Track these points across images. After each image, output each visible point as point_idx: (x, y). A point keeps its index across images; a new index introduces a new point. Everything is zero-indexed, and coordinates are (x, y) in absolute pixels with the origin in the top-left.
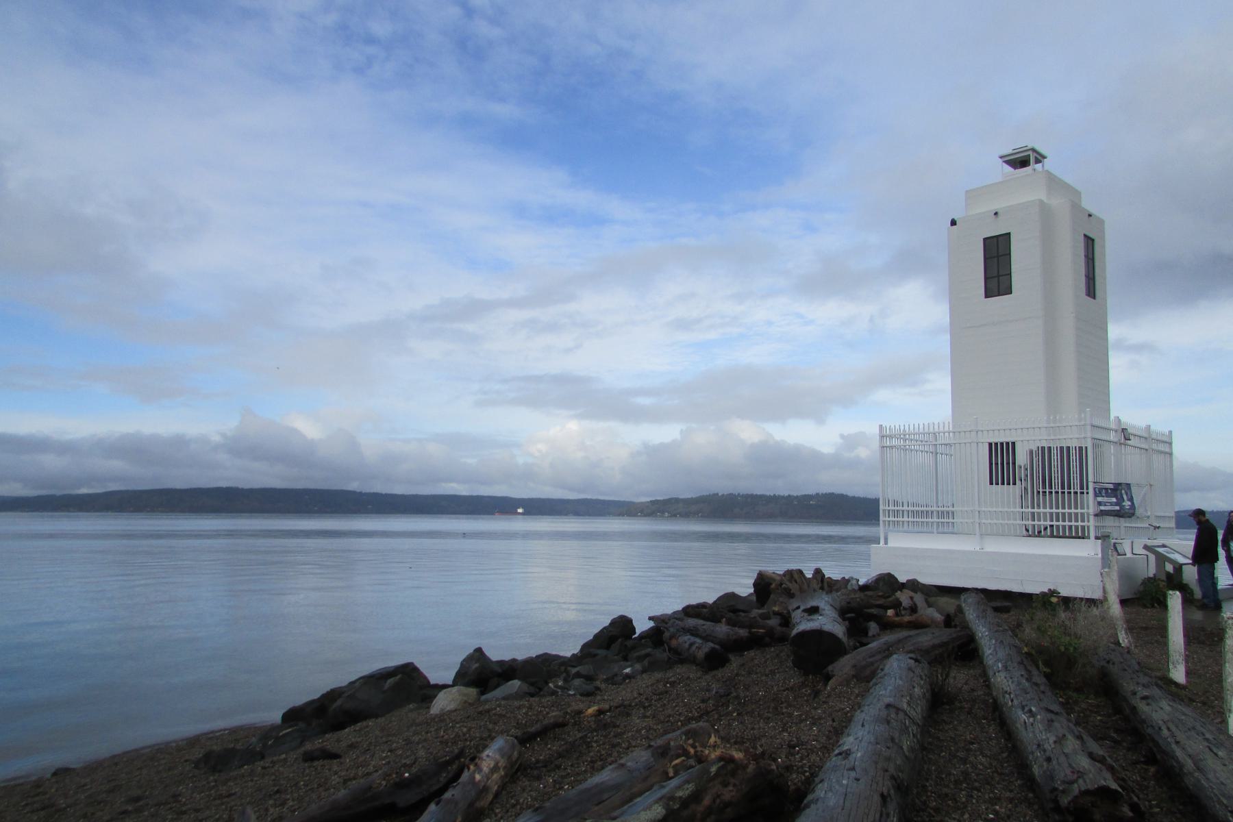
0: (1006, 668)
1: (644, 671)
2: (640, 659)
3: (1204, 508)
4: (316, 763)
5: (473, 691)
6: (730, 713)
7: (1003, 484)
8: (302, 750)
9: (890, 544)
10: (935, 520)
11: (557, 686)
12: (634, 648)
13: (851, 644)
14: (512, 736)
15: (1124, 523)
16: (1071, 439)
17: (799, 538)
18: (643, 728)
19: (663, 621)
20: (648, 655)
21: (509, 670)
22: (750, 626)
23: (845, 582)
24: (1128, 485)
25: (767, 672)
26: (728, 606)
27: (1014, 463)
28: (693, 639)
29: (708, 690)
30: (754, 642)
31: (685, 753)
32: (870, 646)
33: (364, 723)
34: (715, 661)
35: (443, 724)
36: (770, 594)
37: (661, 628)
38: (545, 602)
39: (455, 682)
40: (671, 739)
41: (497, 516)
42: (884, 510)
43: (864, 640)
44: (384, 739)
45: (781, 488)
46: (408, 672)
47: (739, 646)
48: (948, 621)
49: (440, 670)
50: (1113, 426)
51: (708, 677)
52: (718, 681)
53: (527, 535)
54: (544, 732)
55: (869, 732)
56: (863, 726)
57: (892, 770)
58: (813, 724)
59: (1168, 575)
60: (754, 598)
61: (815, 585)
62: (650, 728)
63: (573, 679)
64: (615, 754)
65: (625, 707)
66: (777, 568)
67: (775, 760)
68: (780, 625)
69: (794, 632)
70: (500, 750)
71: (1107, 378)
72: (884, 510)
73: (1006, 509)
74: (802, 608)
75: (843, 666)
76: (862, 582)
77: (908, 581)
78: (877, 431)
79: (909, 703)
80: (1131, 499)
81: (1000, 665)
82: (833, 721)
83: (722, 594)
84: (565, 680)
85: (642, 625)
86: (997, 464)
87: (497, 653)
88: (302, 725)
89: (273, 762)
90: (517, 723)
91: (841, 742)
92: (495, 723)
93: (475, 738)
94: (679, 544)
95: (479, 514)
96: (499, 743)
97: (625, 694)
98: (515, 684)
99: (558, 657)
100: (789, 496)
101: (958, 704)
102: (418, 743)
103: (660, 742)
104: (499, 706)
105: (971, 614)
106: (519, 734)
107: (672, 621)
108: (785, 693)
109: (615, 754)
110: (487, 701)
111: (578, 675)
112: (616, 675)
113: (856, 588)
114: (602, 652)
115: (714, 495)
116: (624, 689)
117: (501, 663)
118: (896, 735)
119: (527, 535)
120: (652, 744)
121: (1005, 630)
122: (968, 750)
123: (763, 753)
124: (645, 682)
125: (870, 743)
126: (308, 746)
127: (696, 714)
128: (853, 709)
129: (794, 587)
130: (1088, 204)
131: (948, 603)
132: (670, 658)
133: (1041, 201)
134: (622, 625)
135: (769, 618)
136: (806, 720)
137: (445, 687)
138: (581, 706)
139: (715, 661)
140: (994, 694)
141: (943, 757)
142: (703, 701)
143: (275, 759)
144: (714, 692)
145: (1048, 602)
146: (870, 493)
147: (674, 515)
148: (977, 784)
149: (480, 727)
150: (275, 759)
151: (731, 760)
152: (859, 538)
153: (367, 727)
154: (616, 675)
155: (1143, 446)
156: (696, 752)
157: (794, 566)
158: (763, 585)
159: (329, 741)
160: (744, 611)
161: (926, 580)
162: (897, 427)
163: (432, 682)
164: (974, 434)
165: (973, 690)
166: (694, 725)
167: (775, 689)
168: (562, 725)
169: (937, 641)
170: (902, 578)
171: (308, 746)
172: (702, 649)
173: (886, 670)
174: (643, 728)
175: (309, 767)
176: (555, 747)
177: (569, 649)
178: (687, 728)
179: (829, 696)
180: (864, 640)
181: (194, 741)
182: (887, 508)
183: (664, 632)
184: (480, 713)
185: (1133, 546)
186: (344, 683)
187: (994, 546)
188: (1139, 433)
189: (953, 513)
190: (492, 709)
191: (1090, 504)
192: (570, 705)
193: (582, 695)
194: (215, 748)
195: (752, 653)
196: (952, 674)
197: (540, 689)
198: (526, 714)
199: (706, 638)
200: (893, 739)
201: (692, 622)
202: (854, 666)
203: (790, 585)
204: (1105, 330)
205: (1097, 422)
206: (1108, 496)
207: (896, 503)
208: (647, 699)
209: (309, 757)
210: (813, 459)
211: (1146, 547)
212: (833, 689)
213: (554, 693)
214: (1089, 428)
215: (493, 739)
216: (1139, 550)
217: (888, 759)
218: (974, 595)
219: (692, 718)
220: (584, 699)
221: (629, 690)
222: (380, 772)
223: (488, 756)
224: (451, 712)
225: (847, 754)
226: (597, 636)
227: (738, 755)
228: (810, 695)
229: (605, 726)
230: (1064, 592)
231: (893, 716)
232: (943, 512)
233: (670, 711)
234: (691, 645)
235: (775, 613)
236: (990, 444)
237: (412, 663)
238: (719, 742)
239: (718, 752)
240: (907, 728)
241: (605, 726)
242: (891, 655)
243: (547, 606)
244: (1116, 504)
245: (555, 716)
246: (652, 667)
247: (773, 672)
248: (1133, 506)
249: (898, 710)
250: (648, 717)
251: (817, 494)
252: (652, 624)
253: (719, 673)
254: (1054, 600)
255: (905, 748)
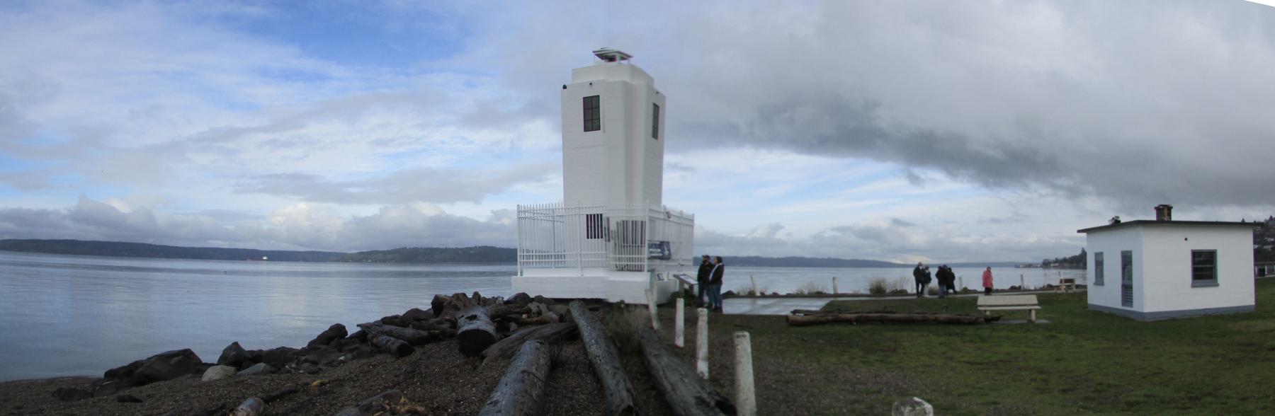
0: (597, 342)
1: (354, 358)
2: (350, 351)
3: (710, 255)
4: (126, 404)
5: (231, 369)
6: (416, 383)
7: (595, 238)
8: (117, 395)
9: (524, 276)
10: (553, 260)
11: (291, 368)
12: (347, 344)
13: (499, 336)
14: (259, 397)
15: (664, 263)
16: (638, 216)
17: (463, 274)
18: (353, 394)
19: (368, 327)
20: (356, 348)
21: (257, 357)
22: (429, 329)
23: (495, 299)
24: (668, 243)
25: (441, 356)
26: (414, 317)
27: (602, 226)
28: (388, 338)
29: (399, 369)
30: (432, 339)
31: (383, 409)
32: (511, 337)
33: (157, 383)
34: (404, 351)
35: (211, 388)
36: (443, 308)
37: (366, 333)
38: (283, 315)
39: (219, 363)
40: (373, 401)
41: (249, 261)
42: (520, 256)
43: (507, 334)
44: (171, 394)
45: (451, 243)
46: (187, 355)
47: (421, 342)
48: (561, 319)
49: (209, 353)
50: (662, 210)
51: (400, 361)
52: (406, 363)
53: (269, 274)
54: (282, 396)
55: (510, 389)
56: (506, 385)
57: (525, 409)
58: (473, 386)
59: (686, 290)
60: (432, 312)
61: (474, 303)
62: (358, 394)
63: (303, 363)
64: (333, 410)
65: (340, 380)
66: (448, 292)
67: (446, 410)
68: (450, 327)
69: (460, 331)
70: (251, 406)
71: (660, 183)
72: (520, 256)
73: (597, 252)
74: (465, 316)
75: (494, 350)
76: (505, 299)
77: (536, 297)
78: (516, 208)
79: (536, 369)
80: (669, 250)
81: (593, 341)
82: (487, 383)
83: (409, 309)
84: (297, 364)
85: (352, 330)
86: (591, 227)
87: (248, 345)
88: (117, 380)
89: (99, 400)
90: (263, 390)
91: (492, 396)
92: (247, 389)
93: (233, 397)
94: (378, 279)
95: (236, 260)
96: (250, 401)
97: (340, 373)
98: (261, 366)
99: (292, 349)
100: (456, 248)
101: (567, 366)
102: (194, 398)
103: (365, 402)
104: (250, 378)
105: (575, 313)
106: (264, 397)
107: (374, 327)
108: (453, 369)
109: (333, 410)
110: (241, 375)
111: (306, 361)
112: (334, 361)
113: (502, 302)
114: (324, 347)
115: (403, 248)
116: (340, 370)
117: (251, 352)
118: (529, 388)
119: (269, 274)
120: (359, 403)
121: (596, 321)
122: (574, 392)
123: (438, 407)
124: (355, 365)
125: (511, 394)
126: (121, 393)
127: (391, 385)
128: (500, 375)
129: (459, 304)
130: (657, 86)
131: (561, 308)
132: (372, 350)
133: (625, 83)
134: (338, 330)
135: (442, 323)
136: (468, 384)
137: (212, 365)
138: (309, 380)
139: (404, 351)
140: (590, 358)
141: (559, 398)
142: (396, 376)
143: (100, 398)
144: (403, 371)
145: (622, 307)
146: (511, 245)
147: (375, 261)
148: (579, 411)
149: (237, 391)
150: (100, 398)
151: (416, 412)
152: (504, 272)
153: (159, 386)
154: (334, 361)
155: (679, 222)
156: (391, 408)
157: (460, 291)
158: (438, 304)
159: (135, 391)
160: (424, 320)
161: (548, 295)
162: (529, 206)
163: (204, 361)
164: (577, 210)
165: (577, 357)
166: (389, 391)
167: (447, 366)
168: (296, 392)
169: (553, 331)
170: (532, 295)
171: (121, 393)
172: (395, 344)
173: (522, 351)
174: (353, 394)
175: (122, 405)
176: (290, 405)
177: (300, 344)
178: (384, 393)
179: (484, 369)
180: (507, 334)
181: (51, 381)
182: (522, 254)
183: (368, 334)
184: (237, 382)
185: (669, 276)
186: (145, 359)
187: (589, 274)
188: (677, 215)
189: (564, 256)
190: (245, 380)
191: (646, 252)
192: (300, 380)
193: (309, 373)
194: (64, 386)
195: (430, 346)
196: (564, 349)
197: (279, 369)
198: (269, 384)
199: (398, 337)
200: (526, 392)
201: (387, 328)
202: (501, 350)
203: (456, 303)
204: (661, 157)
205: (654, 208)
206: (656, 248)
207: (528, 251)
208: (355, 376)
209: (122, 400)
210: (474, 226)
211: (675, 276)
212: (486, 365)
213: (289, 372)
214: (647, 210)
215: (245, 399)
216: (671, 278)
217: (523, 403)
218: (577, 302)
219: (388, 387)
220: (310, 375)
221: (342, 370)
222: (168, 414)
223: (242, 409)
224: (216, 380)
225: (496, 403)
226: (319, 337)
227: (420, 409)
228: (470, 369)
229: (326, 393)
230: (627, 301)
231: (526, 377)
232: (558, 255)
233: (372, 383)
234: (388, 341)
235: (446, 320)
236: (587, 216)
237: (189, 350)
238: (407, 401)
239: (407, 408)
240: (535, 384)
241: (326, 393)
242: (525, 341)
243: (284, 317)
244: (661, 252)
245: (290, 386)
246: (360, 355)
247: (445, 357)
248: (670, 254)
249: (529, 373)
250: (357, 387)
251: (476, 247)
252: (359, 329)
253: (407, 359)
254: (623, 306)
255: (534, 395)
